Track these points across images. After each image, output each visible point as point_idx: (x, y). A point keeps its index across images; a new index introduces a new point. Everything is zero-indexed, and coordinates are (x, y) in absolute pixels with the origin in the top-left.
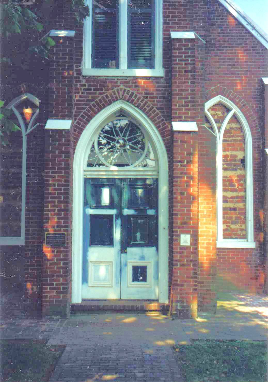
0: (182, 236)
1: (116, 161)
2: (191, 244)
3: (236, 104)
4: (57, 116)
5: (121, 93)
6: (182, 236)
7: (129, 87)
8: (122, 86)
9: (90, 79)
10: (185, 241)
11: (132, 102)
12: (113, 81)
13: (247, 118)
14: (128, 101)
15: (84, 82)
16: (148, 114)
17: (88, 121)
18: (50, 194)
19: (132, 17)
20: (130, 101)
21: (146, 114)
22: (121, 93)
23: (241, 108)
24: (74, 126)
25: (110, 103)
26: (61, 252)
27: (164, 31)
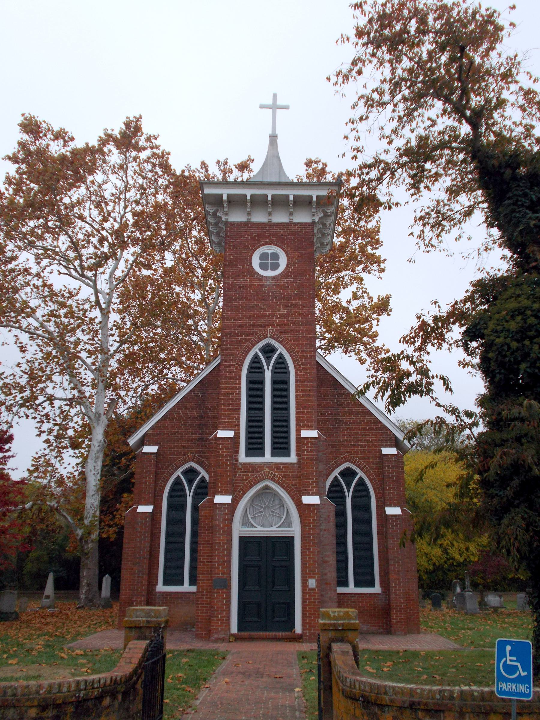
0: (310, 580)
1: (159, 323)
2: (317, 586)
3: (362, 470)
4: (222, 493)
5: (266, 474)
6: (310, 580)
7: (272, 470)
8: (267, 470)
9: (244, 464)
10: (312, 584)
11: (274, 481)
12: (261, 466)
13: (371, 481)
14: (272, 480)
15: (240, 467)
16: (285, 489)
17: (244, 494)
18: (216, 550)
19: (274, 382)
20: (273, 480)
21: (285, 489)
22: (266, 474)
23: (365, 473)
24: (233, 500)
25: (259, 481)
26: (225, 593)
27: (297, 430)
